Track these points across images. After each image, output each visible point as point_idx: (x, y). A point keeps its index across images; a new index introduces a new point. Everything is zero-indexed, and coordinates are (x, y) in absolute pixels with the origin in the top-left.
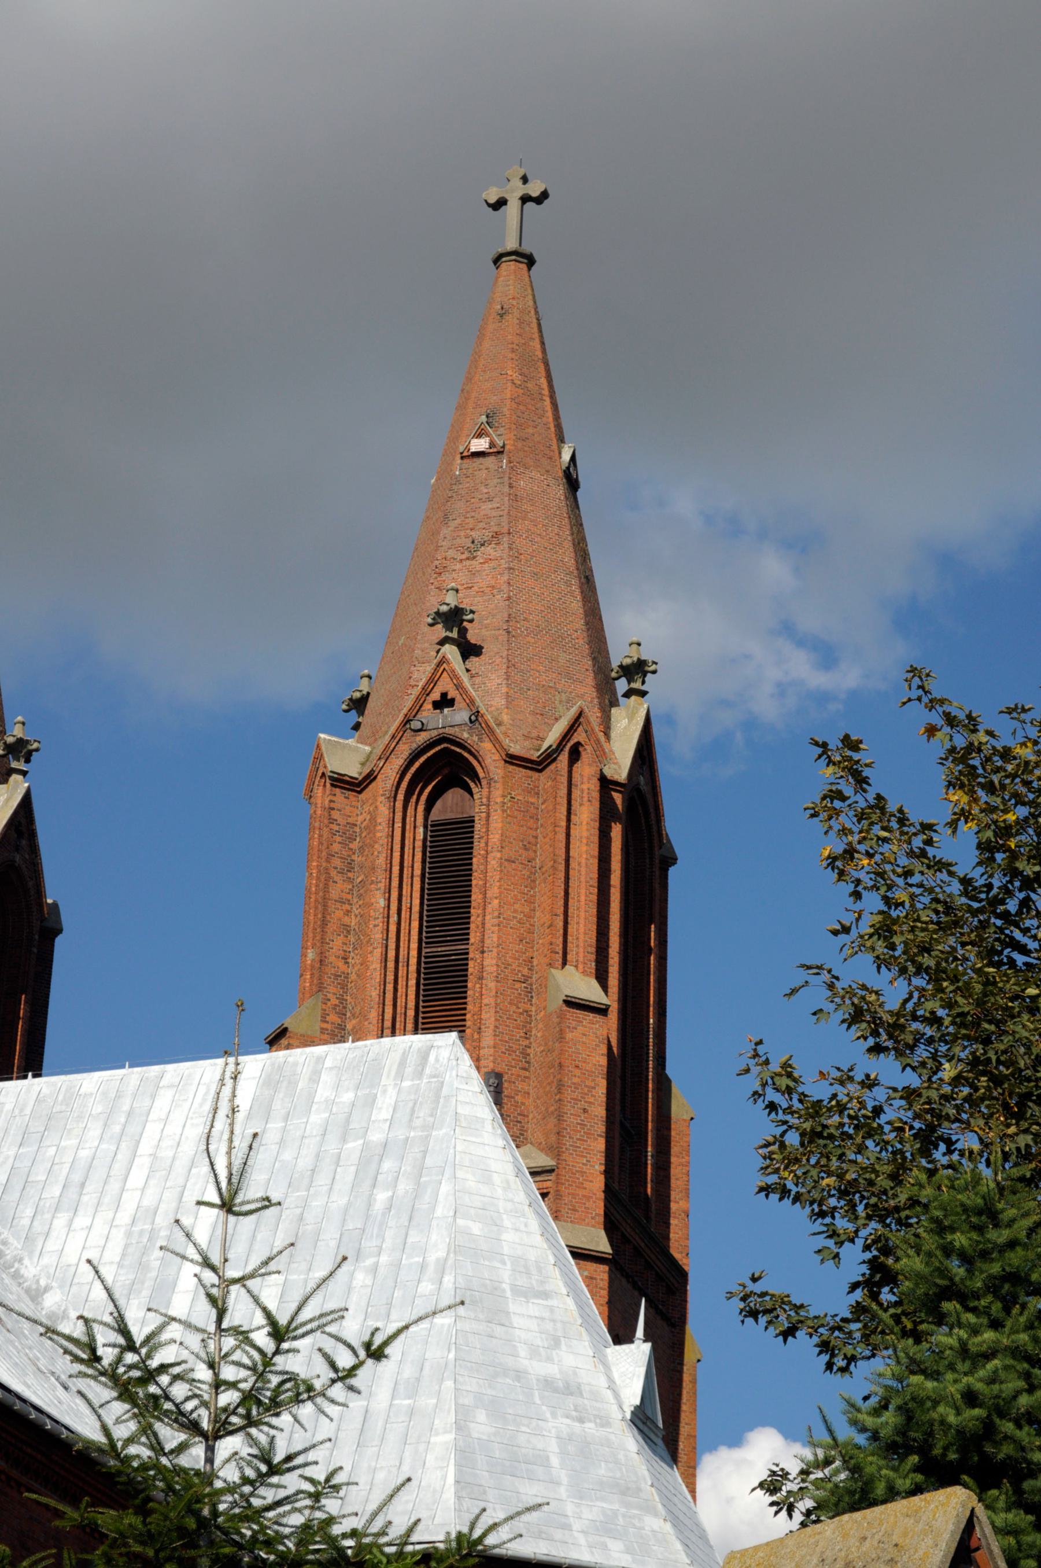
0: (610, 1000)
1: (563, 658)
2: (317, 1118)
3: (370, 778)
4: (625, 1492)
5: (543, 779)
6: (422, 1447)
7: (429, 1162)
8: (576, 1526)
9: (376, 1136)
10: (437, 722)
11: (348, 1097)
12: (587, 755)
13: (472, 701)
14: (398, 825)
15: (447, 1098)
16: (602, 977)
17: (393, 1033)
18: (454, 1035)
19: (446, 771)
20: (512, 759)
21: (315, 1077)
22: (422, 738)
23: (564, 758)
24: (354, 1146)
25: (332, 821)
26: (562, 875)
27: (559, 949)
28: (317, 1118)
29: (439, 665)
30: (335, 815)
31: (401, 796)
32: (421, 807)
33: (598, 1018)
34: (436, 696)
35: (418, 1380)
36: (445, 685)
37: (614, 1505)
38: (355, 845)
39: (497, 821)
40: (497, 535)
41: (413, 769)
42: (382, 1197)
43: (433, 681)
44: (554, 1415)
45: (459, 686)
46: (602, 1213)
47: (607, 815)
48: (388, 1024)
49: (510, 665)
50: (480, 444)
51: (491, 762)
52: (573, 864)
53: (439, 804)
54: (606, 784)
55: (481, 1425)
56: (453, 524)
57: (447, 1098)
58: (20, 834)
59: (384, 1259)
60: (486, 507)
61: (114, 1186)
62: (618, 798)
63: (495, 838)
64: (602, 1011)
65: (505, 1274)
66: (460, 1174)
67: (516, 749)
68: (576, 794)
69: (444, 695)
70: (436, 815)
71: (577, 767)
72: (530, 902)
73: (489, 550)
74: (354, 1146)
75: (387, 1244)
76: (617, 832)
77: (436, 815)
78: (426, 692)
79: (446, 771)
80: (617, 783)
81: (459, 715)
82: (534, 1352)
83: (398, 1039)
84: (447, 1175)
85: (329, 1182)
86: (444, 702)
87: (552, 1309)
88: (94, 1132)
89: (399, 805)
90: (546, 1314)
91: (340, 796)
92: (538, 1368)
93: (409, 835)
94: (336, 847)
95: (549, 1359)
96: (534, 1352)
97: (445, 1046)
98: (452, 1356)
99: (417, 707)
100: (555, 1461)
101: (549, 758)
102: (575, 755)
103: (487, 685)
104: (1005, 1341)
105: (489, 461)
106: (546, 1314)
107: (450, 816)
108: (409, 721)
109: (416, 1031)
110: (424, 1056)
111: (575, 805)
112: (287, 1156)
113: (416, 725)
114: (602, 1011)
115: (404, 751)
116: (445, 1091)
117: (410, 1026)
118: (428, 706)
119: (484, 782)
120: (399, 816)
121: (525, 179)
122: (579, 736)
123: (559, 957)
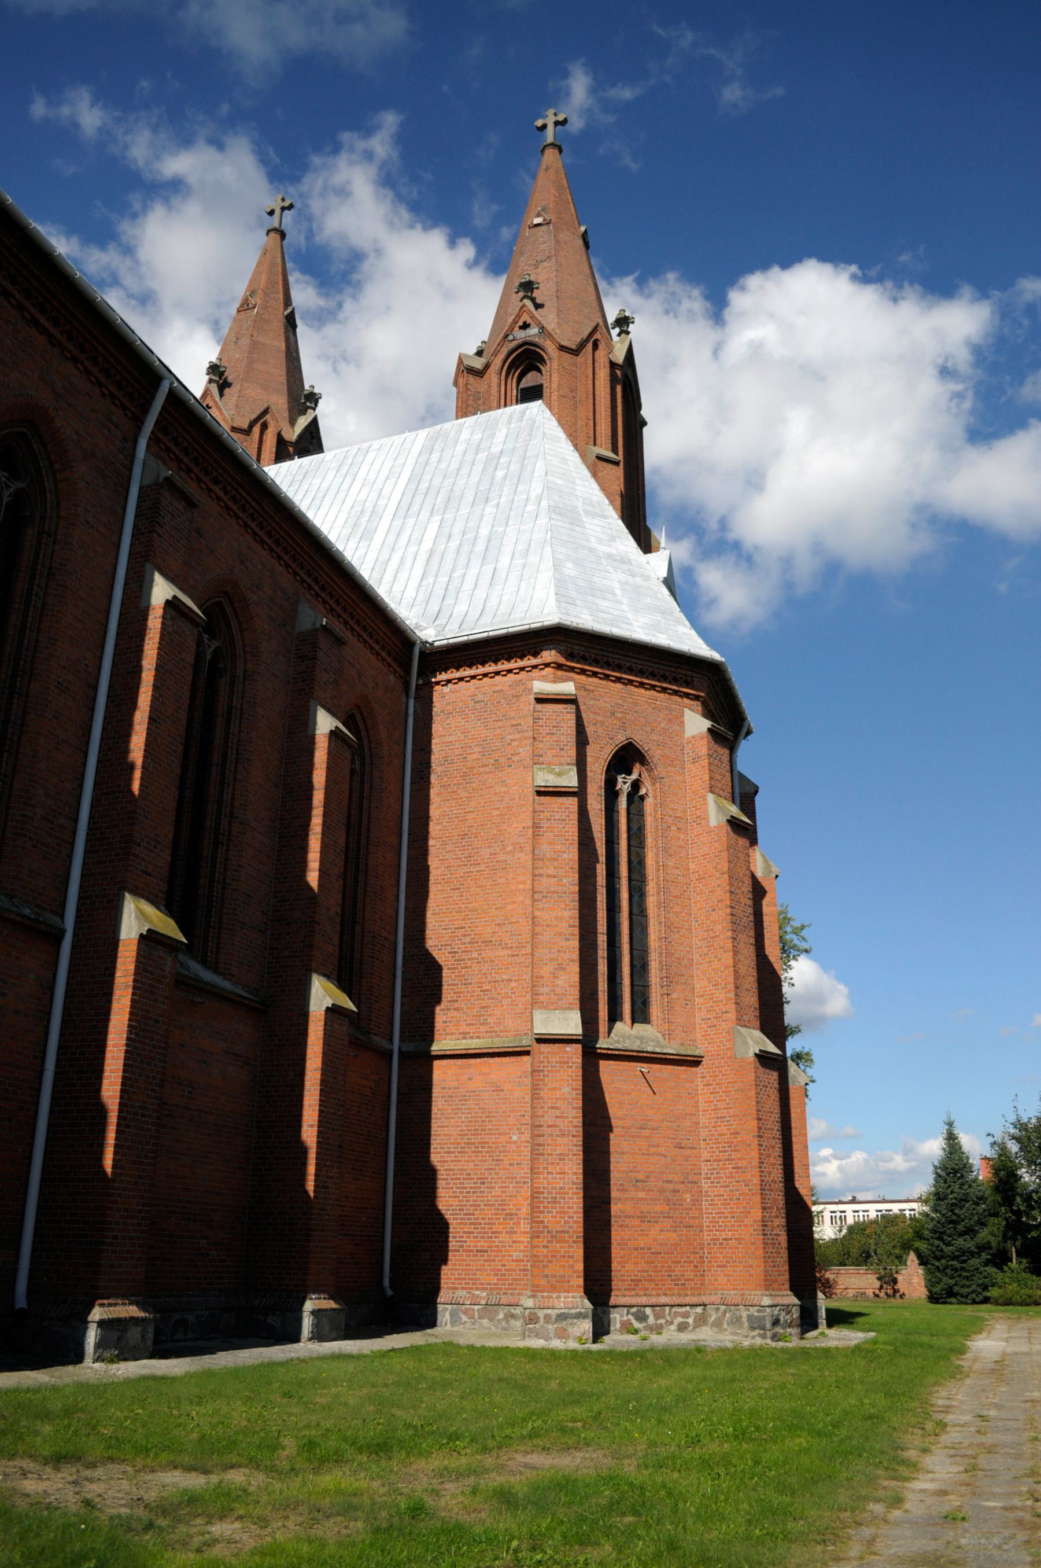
0: (620, 457)
1: (586, 311)
2: (460, 448)
3: (487, 366)
4: (663, 613)
5: (580, 359)
6: (532, 581)
7: (528, 454)
8: (635, 624)
9: (496, 449)
10: (521, 335)
11: (478, 436)
12: (602, 346)
13: (540, 323)
14: (503, 387)
15: (538, 427)
16: (615, 450)
17: (505, 405)
18: (540, 401)
19: (527, 362)
20: (562, 348)
21: (459, 432)
22: (514, 344)
23: (590, 346)
24: (482, 456)
25: (468, 390)
26: (591, 401)
27: (592, 436)
28: (460, 448)
29: (522, 308)
30: (469, 387)
31: (504, 374)
32: (515, 380)
33: (614, 467)
34: (521, 323)
35: (528, 550)
36: (525, 318)
37: (659, 617)
38: (480, 402)
39: (555, 377)
40: (549, 257)
41: (510, 360)
42: (500, 474)
43: (519, 316)
44: (616, 571)
45: (532, 317)
46: (576, 810)
47: (614, 380)
48: (503, 401)
49: (559, 310)
50: (538, 220)
51: (551, 348)
52: (597, 398)
53: (524, 380)
54: (613, 365)
55: (570, 569)
56: (526, 256)
57: (538, 427)
58: (311, 433)
59: (503, 500)
60: (543, 246)
61: (342, 495)
62: (619, 373)
63: (555, 386)
64: (617, 463)
65: (580, 505)
66: (548, 457)
67: (564, 343)
68: (597, 365)
69: (525, 323)
70: (522, 386)
71: (597, 353)
72: (575, 417)
73: (546, 264)
74: (482, 456)
75: (505, 492)
76: (619, 389)
77: (522, 386)
78: (515, 322)
79: (527, 362)
80: (617, 365)
81: (534, 331)
82: (600, 541)
83: (507, 409)
84: (540, 457)
85: (472, 587)
86: (525, 326)
87: (609, 523)
88: (331, 475)
89: (503, 378)
90: (606, 525)
91: (472, 379)
92: (604, 549)
93: (509, 394)
94: (470, 402)
95: (609, 546)
96: (600, 541)
97: (536, 408)
98: (549, 536)
99: (511, 329)
100: (618, 592)
101: (582, 345)
102: (596, 345)
103: (548, 318)
104: (305, 1549)
105: (544, 228)
106: (606, 525)
107: (530, 385)
108: (507, 336)
109: (517, 403)
110: (523, 414)
111: (597, 370)
112: (443, 466)
113: (511, 337)
114: (617, 463)
115: (504, 351)
116: (536, 424)
117: (514, 401)
118: (517, 328)
119: (548, 362)
120: (503, 382)
121: (555, 114)
122: (597, 336)
123: (592, 440)
